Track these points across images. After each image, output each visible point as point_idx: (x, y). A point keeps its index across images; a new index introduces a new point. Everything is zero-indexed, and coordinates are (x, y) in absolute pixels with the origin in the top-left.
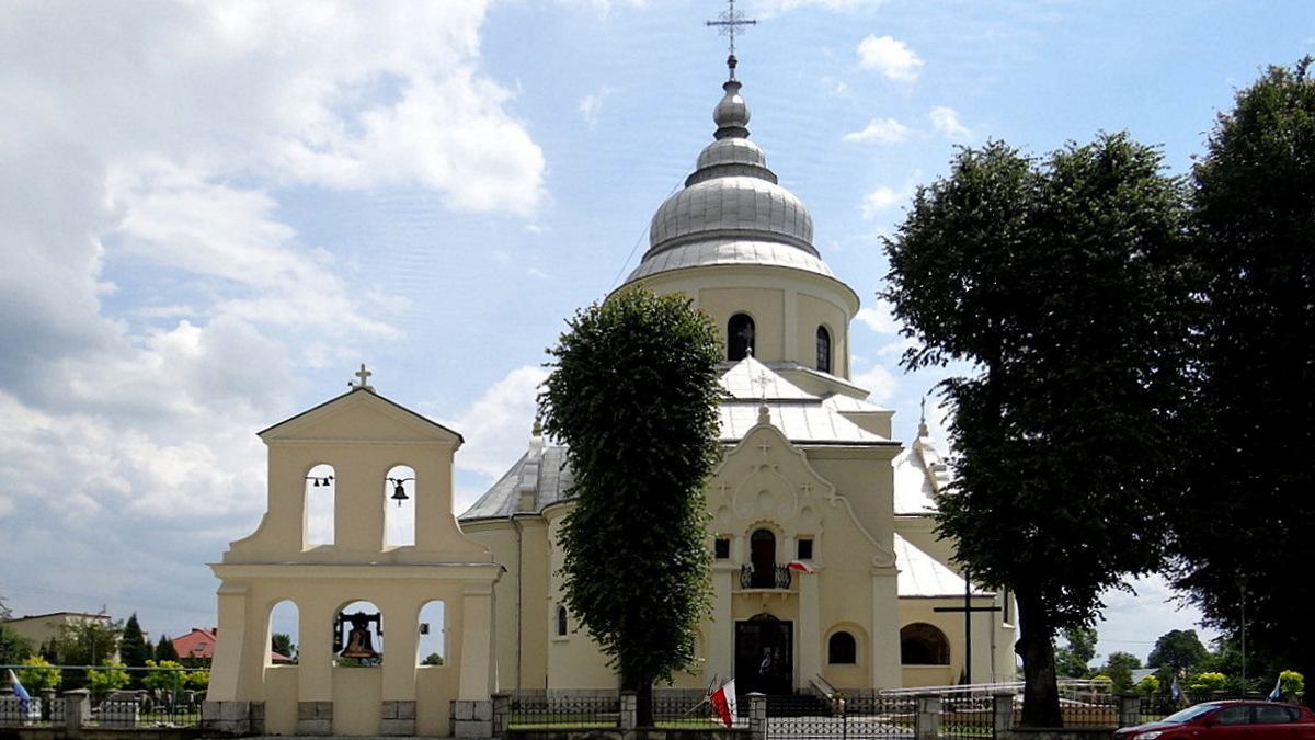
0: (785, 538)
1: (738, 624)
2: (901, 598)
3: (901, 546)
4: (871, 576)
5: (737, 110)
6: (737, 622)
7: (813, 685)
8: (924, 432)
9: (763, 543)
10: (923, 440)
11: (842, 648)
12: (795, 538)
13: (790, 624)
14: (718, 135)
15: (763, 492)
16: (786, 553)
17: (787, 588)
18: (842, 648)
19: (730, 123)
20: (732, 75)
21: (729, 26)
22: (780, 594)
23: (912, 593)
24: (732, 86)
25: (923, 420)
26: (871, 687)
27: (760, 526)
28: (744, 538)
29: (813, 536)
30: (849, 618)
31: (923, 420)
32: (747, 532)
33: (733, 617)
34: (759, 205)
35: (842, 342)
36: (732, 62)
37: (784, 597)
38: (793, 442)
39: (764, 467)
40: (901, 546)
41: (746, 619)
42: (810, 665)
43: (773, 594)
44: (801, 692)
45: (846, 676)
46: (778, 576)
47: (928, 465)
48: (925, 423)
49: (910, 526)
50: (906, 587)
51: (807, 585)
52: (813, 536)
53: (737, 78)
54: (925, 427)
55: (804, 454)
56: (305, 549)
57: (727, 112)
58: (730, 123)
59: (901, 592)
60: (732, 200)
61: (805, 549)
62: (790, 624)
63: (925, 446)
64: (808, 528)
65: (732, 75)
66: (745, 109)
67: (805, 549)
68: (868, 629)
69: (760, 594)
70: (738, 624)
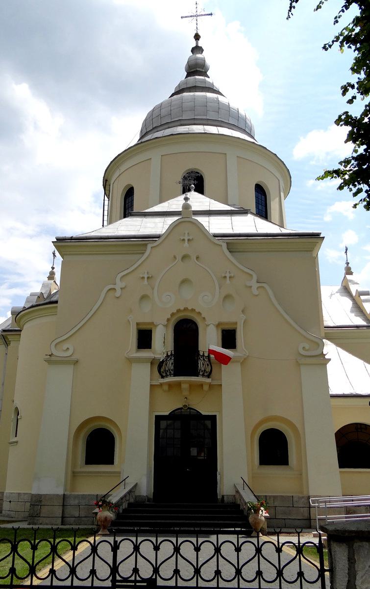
0: (208, 325)
1: (159, 419)
2: (333, 396)
3: (330, 349)
4: (298, 365)
5: (199, 61)
6: (157, 417)
7: (237, 492)
8: (349, 271)
9: (186, 331)
10: (349, 277)
11: (273, 447)
12: (218, 326)
13: (213, 419)
15: (184, 281)
16: (209, 341)
17: (209, 376)
18: (273, 447)
19: (196, 69)
20: (197, 43)
21: (195, 18)
22: (201, 385)
23: (347, 392)
24: (197, 49)
25: (348, 263)
26: (305, 494)
27: (182, 315)
28: (166, 326)
29: (236, 323)
30: (279, 412)
31: (348, 263)
32: (168, 320)
33: (151, 410)
34: (209, 104)
35: (277, 199)
36: (197, 37)
37: (206, 388)
38: (215, 236)
39: (185, 257)
40: (330, 349)
41: (167, 413)
42: (236, 467)
43: (192, 387)
44: (225, 498)
45: (277, 481)
46: (201, 365)
47: (354, 294)
48: (350, 265)
49: (342, 336)
50: (338, 384)
51: (230, 377)
52: (236, 323)
54: (350, 269)
55: (224, 246)
56: (152, 497)
57: (193, 62)
58: (196, 69)
59: (334, 390)
60: (191, 102)
61: (229, 338)
62: (213, 419)
63: (351, 281)
64: (230, 316)
65: (197, 43)
66: (205, 61)
67: (229, 338)
68: (298, 426)
69: (179, 384)
70: (159, 419)
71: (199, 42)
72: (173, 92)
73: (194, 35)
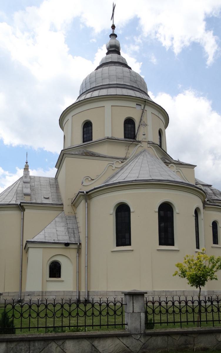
14: (107, 54)
19: (114, 49)
24: (113, 27)
53: (115, 33)
58: (114, 49)
71: (115, 30)
72: (98, 65)
73: (111, 26)
